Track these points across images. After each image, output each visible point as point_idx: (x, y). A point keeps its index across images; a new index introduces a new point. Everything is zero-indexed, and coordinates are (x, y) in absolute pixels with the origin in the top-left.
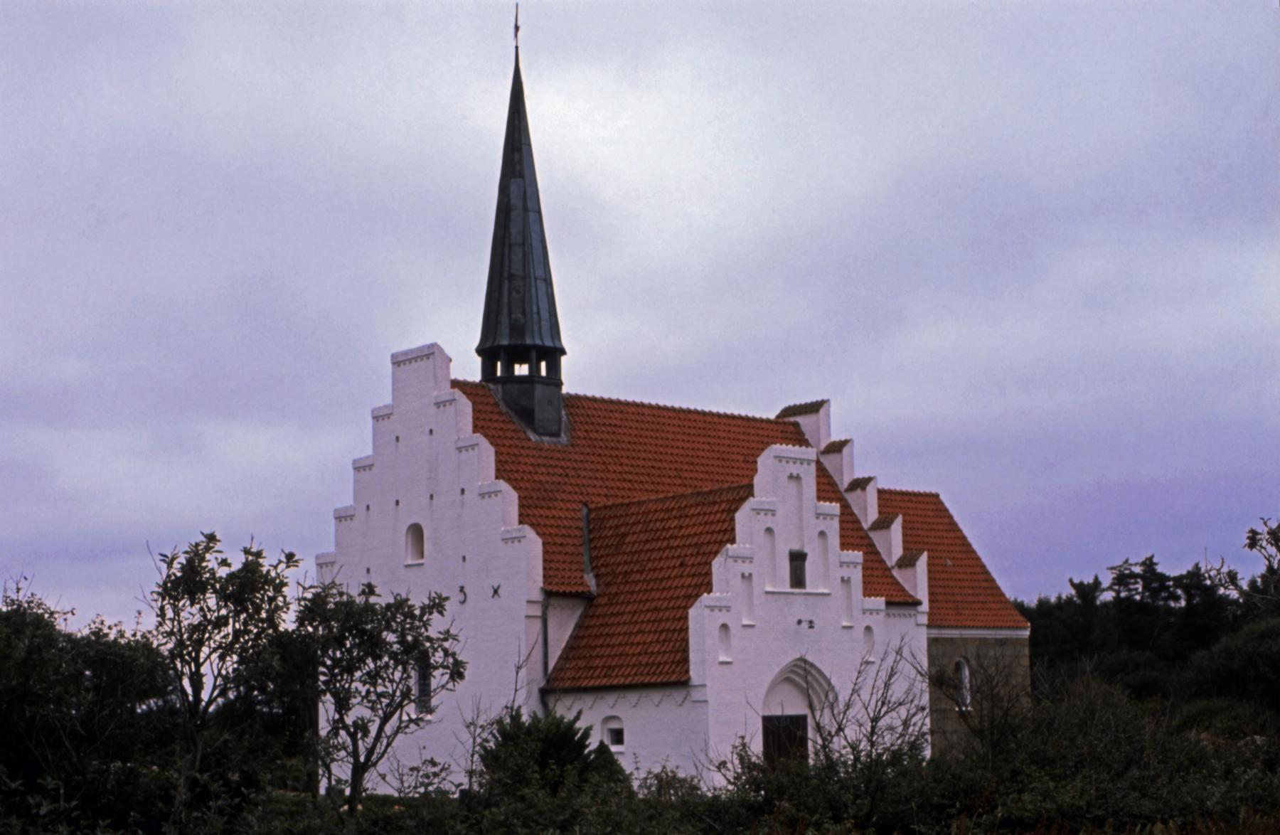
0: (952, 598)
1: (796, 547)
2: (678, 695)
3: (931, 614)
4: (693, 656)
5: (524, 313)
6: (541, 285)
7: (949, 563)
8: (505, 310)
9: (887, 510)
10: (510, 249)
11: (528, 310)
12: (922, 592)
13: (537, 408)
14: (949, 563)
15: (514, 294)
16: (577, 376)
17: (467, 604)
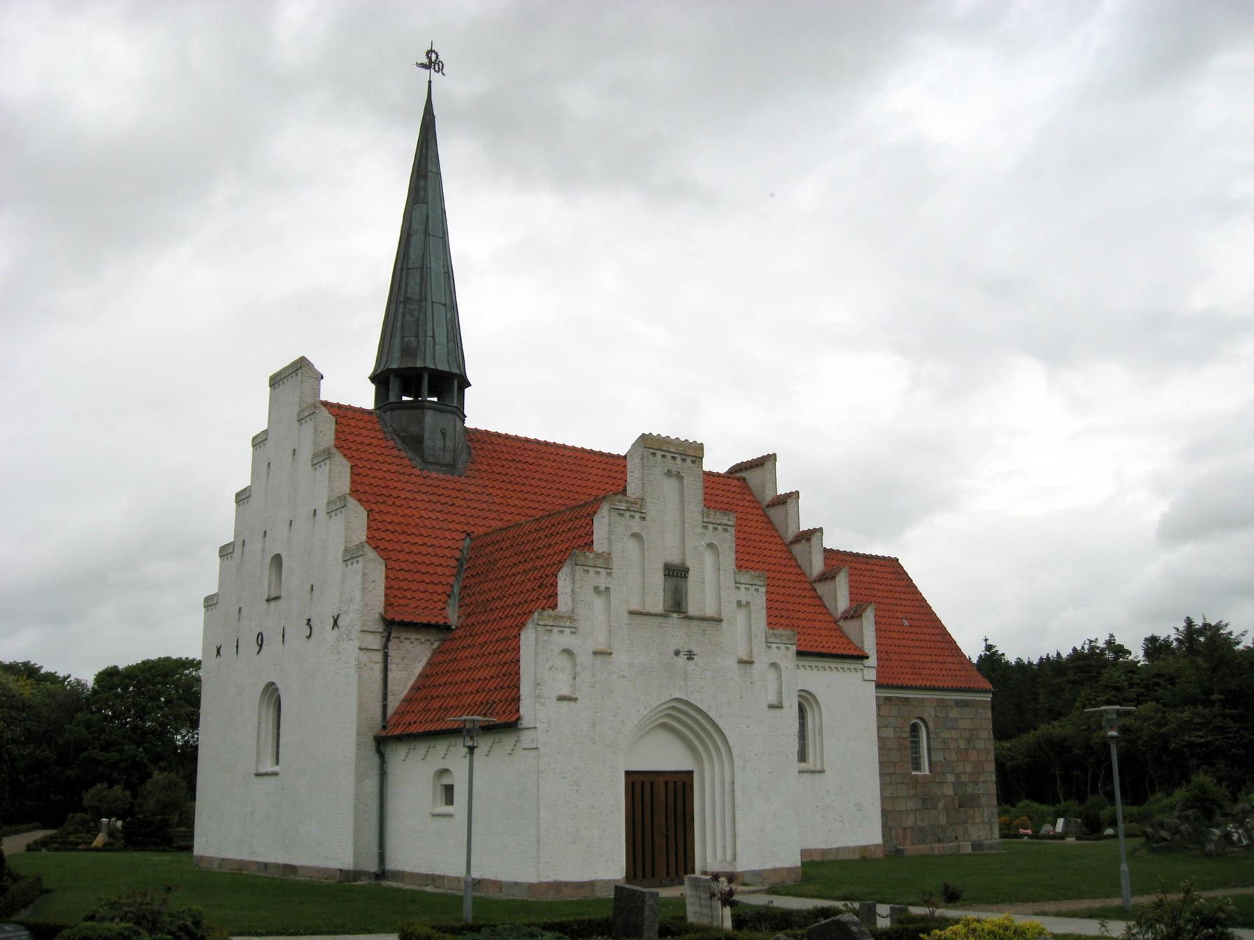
0: (908, 657)
1: (674, 558)
2: (508, 741)
3: (880, 669)
4: (526, 689)
5: (417, 337)
6: (440, 314)
7: (906, 623)
8: (398, 334)
9: (833, 562)
10: (408, 274)
11: (421, 334)
12: (870, 645)
13: (427, 435)
14: (906, 623)
15: (408, 316)
16: (485, 409)
17: (313, 638)
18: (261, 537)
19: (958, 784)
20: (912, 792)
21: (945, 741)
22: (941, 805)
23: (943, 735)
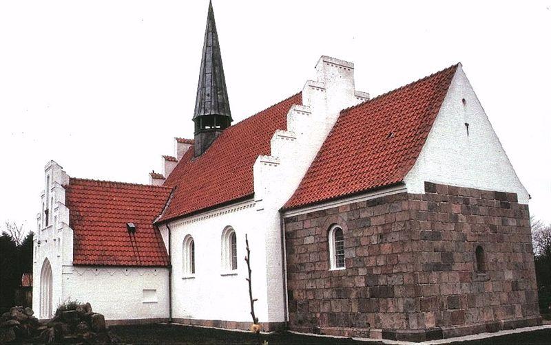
18: (462, 103)
19: (370, 276)
20: (328, 285)
21: (357, 240)
22: (353, 296)
23: (355, 235)
